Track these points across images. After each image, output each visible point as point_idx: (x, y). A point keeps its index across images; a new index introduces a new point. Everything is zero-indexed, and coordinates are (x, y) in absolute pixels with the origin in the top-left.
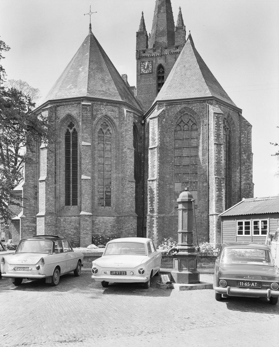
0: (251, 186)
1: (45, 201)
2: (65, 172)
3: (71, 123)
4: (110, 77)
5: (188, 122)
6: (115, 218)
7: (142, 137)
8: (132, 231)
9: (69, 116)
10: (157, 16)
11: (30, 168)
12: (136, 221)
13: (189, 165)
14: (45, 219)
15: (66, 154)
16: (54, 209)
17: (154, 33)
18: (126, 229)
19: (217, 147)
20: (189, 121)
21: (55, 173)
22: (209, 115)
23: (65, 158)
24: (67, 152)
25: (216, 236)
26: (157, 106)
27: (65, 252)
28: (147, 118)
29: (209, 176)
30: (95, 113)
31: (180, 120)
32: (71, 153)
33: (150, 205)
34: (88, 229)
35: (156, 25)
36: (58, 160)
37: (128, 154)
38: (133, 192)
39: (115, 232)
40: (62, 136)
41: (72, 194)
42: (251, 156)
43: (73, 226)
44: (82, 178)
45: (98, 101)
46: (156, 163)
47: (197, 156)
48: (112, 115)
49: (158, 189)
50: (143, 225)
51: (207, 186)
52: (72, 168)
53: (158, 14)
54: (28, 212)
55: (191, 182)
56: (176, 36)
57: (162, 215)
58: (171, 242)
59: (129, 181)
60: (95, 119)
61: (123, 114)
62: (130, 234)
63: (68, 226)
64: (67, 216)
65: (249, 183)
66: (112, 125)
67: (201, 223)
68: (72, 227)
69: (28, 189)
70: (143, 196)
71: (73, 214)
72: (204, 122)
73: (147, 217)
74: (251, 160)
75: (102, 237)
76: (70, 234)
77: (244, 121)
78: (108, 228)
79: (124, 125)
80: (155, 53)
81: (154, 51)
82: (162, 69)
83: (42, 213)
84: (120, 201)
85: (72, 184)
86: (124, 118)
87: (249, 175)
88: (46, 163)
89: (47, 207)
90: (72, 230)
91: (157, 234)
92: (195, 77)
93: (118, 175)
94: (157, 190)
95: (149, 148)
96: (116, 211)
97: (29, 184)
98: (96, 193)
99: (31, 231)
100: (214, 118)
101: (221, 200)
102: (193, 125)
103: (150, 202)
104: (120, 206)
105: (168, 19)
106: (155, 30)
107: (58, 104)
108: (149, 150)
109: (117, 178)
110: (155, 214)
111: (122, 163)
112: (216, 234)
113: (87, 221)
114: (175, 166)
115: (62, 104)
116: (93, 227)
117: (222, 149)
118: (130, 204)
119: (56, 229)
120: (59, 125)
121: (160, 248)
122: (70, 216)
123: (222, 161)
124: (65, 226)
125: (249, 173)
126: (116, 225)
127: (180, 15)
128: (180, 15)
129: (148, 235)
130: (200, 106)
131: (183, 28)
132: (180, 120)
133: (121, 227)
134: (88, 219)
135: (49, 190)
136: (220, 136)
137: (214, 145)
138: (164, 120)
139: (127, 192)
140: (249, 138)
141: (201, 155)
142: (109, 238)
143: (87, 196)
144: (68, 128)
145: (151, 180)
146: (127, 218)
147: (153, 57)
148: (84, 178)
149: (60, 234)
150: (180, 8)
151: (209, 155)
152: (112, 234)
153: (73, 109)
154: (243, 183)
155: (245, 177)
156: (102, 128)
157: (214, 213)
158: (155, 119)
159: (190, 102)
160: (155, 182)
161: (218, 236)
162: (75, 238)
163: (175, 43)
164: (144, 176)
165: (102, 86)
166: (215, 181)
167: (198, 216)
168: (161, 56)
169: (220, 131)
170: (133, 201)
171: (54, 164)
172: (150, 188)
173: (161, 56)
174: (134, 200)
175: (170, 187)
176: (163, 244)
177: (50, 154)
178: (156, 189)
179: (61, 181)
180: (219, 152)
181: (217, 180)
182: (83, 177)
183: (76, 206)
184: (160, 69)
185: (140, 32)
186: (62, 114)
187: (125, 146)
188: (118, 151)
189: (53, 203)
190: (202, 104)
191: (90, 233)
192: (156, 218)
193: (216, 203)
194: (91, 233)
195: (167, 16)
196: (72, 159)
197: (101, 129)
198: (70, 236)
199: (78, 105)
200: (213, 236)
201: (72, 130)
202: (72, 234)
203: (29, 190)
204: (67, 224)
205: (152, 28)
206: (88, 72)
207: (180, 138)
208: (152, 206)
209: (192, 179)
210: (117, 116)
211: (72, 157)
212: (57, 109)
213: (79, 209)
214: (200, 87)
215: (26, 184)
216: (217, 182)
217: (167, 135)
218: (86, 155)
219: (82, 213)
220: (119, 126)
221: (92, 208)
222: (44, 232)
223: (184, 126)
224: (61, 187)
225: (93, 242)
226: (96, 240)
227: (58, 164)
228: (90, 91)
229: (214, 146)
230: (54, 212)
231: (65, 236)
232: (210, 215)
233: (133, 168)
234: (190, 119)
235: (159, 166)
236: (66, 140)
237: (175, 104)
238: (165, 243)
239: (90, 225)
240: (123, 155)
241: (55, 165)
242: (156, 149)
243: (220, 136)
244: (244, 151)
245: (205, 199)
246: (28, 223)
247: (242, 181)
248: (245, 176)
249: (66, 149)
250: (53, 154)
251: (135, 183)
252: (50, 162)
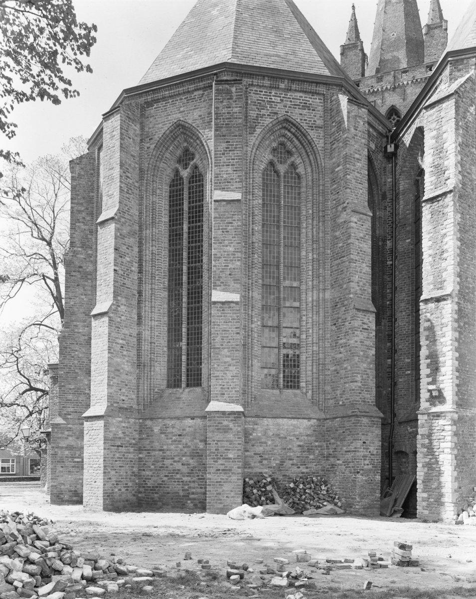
1: (107, 373)
2: (169, 292)
3: (186, 150)
4: (298, 26)
6: (313, 422)
7: (389, 196)
8: (367, 462)
9: (182, 130)
10: (385, 12)
11: (80, 290)
12: (378, 431)
14: (106, 426)
15: (170, 241)
16: (134, 397)
17: (378, 47)
18: (349, 456)
21: (140, 293)
23: (167, 252)
24: (174, 236)
30: (253, 114)
32: (185, 236)
33: (430, 379)
34: (231, 456)
36: (147, 257)
37: (353, 228)
38: (368, 343)
39: (313, 467)
40: (161, 189)
41: (188, 355)
43: (186, 446)
44: (214, 299)
45: (264, 76)
46: (451, 244)
48: (305, 120)
49: (456, 325)
50: (393, 446)
52: (189, 278)
53: (385, 7)
54: (72, 409)
59: (358, 310)
60: (255, 131)
61: (339, 111)
62: (361, 472)
63: (172, 447)
64: (172, 419)
66: (303, 151)
68: (185, 450)
69: (72, 346)
70: (390, 360)
71: (188, 412)
73: (420, 417)
75: (273, 479)
76: (179, 470)
78: (292, 454)
80: (382, 83)
82: (395, 117)
83: (98, 407)
84: (329, 373)
85: (188, 324)
86: (341, 122)
88: (112, 264)
89: (111, 391)
90: (184, 458)
91: (456, 473)
93: (321, 295)
94: (454, 330)
96: (314, 402)
97: (77, 335)
98: (257, 349)
99: (78, 462)
103: (428, 371)
105: (407, 15)
107: (149, 98)
108: (423, 204)
109: (317, 304)
111: (334, 258)
113: (227, 430)
115: (159, 95)
116: (248, 451)
118: (359, 378)
119: (141, 456)
120: (150, 159)
121: (465, 522)
122: (178, 418)
124: (165, 447)
126: (317, 444)
129: (422, 478)
131: (441, 26)
133: (331, 451)
134: (231, 425)
135: (121, 341)
139: (352, 342)
142: (295, 483)
143: (228, 354)
144: (177, 165)
146: (350, 424)
147: (376, 92)
148: (219, 300)
149: (151, 470)
152: (305, 470)
153: (191, 105)
156: (276, 160)
160: (449, 302)
162: (194, 482)
164: (392, 305)
165: (274, 45)
168: (395, 88)
170: (369, 371)
171: (135, 267)
172: (427, 324)
173: (395, 88)
174: (370, 369)
177: (123, 237)
178: (450, 327)
179: (156, 316)
182: (218, 295)
183: (198, 390)
184: (392, 118)
186: (160, 126)
187: (345, 205)
188: (321, 224)
189: (132, 379)
191: (237, 468)
192: (452, 420)
194: (239, 468)
195: (405, 9)
196: (189, 253)
197: (271, 163)
198: (178, 476)
199: (206, 93)
201: (188, 170)
202: (185, 469)
203: (76, 351)
204: (170, 441)
205: (374, 39)
206: (235, 14)
210: (320, 122)
211: (189, 249)
212: (147, 113)
213: (205, 395)
215: (66, 334)
218: (226, 231)
219: (214, 406)
220: (325, 149)
221: (244, 393)
222: (102, 465)
224: (157, 333)
225: (248, 499)
226: (255, 491)
227: (147, 267)
228: (239, 55)
230: (135, 406)
231: (166, 476)
233: (369, 270)
235: (458, 251)
236: (170, 201)
239: (239, 442)
240: (337, 234)
241: (140, 272)
246: (70, 438)
249: (170, 226)
250: (132, 241)
251: (374, 315)
252: (124, 260)
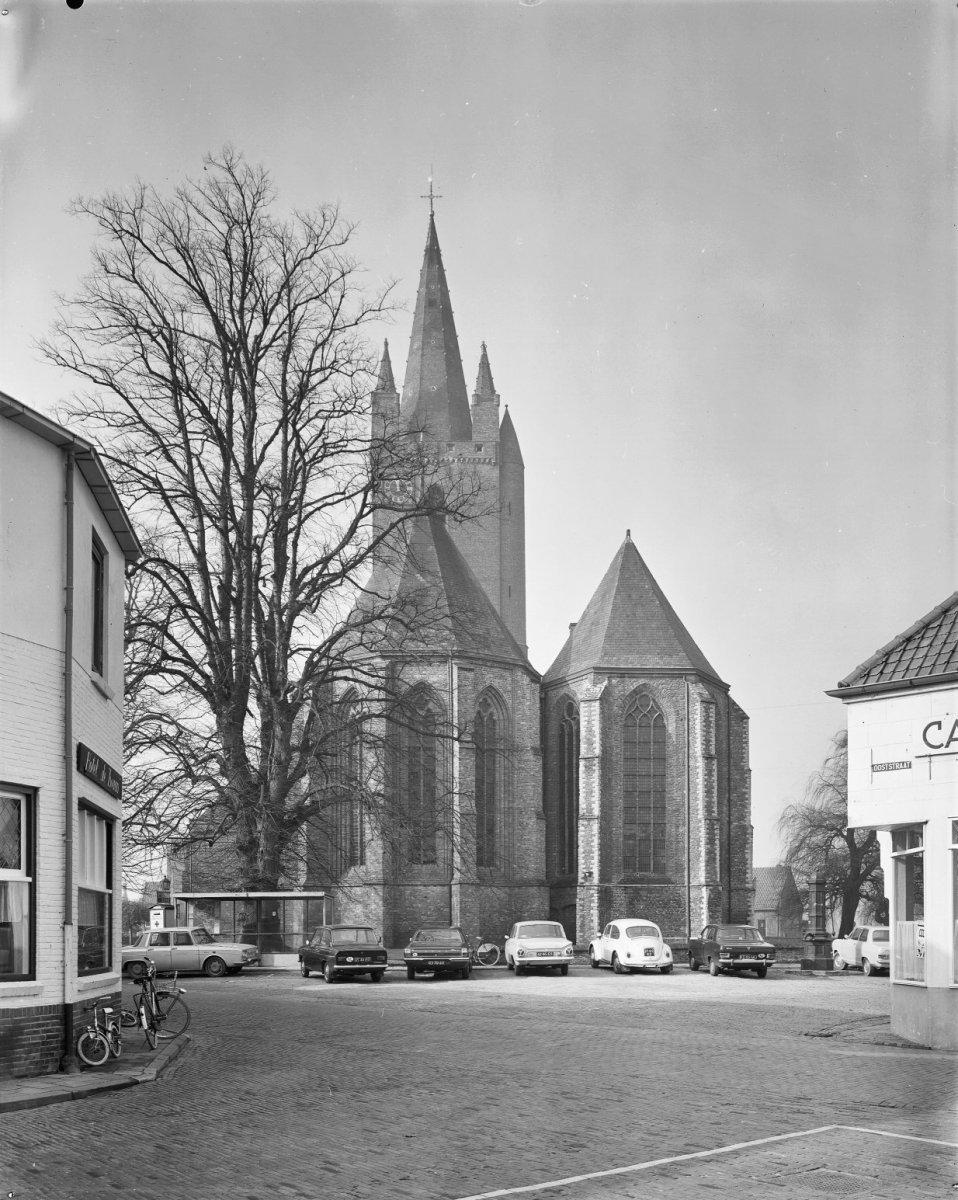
27: (312, 977)
35: (418, 373)
101: (715, 859)
127: (485, 365)
128: (485, 365)
150: (484, 347)
158: (593, 704)
193: (707, 866)
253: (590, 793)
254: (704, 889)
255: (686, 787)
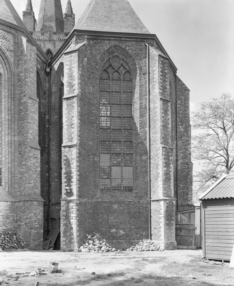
0: (189, 167)
5: (119, 68)
6: (9, 203)
7: (47, 93)
8: (36, 223)
12: (42, 208)
13: (121, 130)
18: (28, 220)
19: (163, 104)
20: (120, 66)
22: (150, 59)
25: (164, 231)
26: (74, 39)
28: (54, 64)
29: (150, 146)
31: (107, 64)
33: (66, 184)
35: (44, 9)
38: (37, 164)
42: (189, 129)
46: (76, 121)
47: (132, 117)
48: (4, 45)
49: (78, 159)
50: (49, 216)
51: (178, 150)
55: (124, 154)
56: (65, 23)
57: (84, 201)
58: (99, 240)
59: (32, 148)
61: (22, 45)
62: (34, 228)
65: (187, 162)
67: (140, 213)
70: (47, 174)
72: (142, 69)
73: (62, 202)
74: (189, 134)
77: (180, 83)
79: (23, 62)
81: (43, 34)
82: (50, 55)
87: (186, 153)
92: (125, 12)
93: (13, 138)
94: (77, 161)
95: (64, 97)
100: (159, 63)
101: (170, 179)
102: (125, 72)
103: (65, 180)
104: (16, 186)
105: (56, 6)
106: (43, 15)
110: (74, 197)
111: (19, 120)
112: (164, 227)
114: (101, 130)
117: (169, 108)
118: (32, 182)
123: (168, 124)
125: (187, 149)
126: (11, 214)
128: (69, 3)
129: (63, 231)
130: (136, 46)
131: (72, 16)
132: (107, 65)
136: (166, 90)
137: (160, 100)
138: (86, 59)
139: (29, 163)
140: (186, 105)
141: (138, 115)
145: (67, 146)
147: (41, 40)
151: (151, 116)
152: (5, 228)
154: (180, 162)
155: (182, 155)
157: (161, 197)
158: (73, 54)
159: (122, 39)
160: (75, 148)
161: (166, 231)
163: (64, 30)
166: (161, 152)
167: (135, 202)
168: (50, 40)
169: (166, 83)
170: (37, 179)
172: (65, 158)
173: (50, 40)
174: (38, 178)
175: (93, 158)
176: (87, 244)
178: (75, 160)
180: (165, 112)
181: (165, 151)
184: (49, 55)
185: (26, 12)
187: (25, 94)
188: (12, 101)
190: (139, 44)
192: (76, 203)
193: (164, 184)
195: (55, 3)
200: (160, 231)
207: (107, 91)
208: (69, 185)
209: (125, 150)
210: (12, 48)
214: (134, 24)
216: (164, 153)
217: (89, 82)
223: (113, 73)
229: (159, 101)
232: (153, 201)
233: (37, 128)
234: (122, 65)
237: (101, 38)
238: (91, 242)
240: (21, 108)
242: (75, 99)
243: (166, 90)
244: (181, 121)
245: (144, 178)
247: (178, 160)
248: (182, 153)
251: (40, 151)
253: (71, 125)
254: (162, 203)
255: (148, 126)
